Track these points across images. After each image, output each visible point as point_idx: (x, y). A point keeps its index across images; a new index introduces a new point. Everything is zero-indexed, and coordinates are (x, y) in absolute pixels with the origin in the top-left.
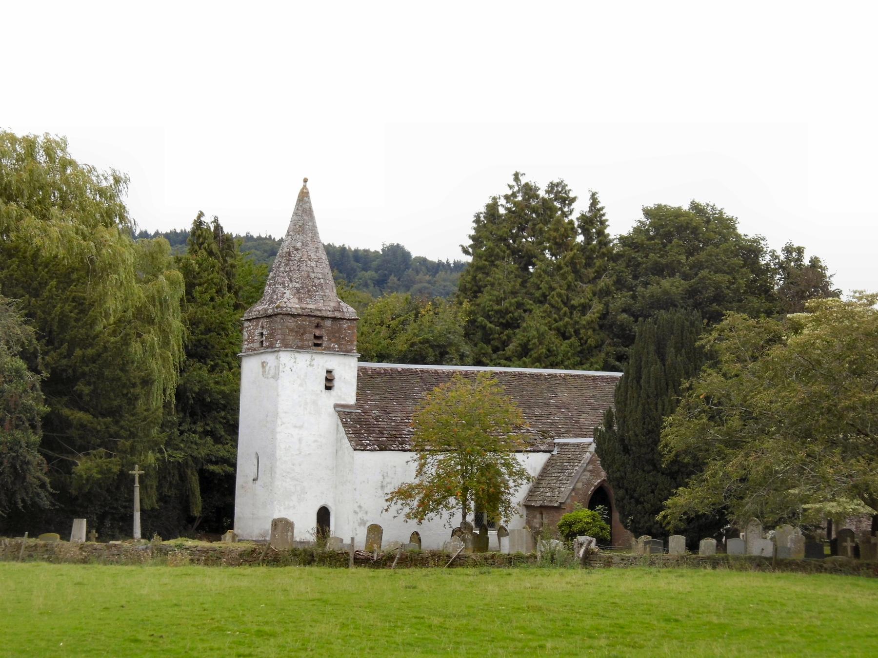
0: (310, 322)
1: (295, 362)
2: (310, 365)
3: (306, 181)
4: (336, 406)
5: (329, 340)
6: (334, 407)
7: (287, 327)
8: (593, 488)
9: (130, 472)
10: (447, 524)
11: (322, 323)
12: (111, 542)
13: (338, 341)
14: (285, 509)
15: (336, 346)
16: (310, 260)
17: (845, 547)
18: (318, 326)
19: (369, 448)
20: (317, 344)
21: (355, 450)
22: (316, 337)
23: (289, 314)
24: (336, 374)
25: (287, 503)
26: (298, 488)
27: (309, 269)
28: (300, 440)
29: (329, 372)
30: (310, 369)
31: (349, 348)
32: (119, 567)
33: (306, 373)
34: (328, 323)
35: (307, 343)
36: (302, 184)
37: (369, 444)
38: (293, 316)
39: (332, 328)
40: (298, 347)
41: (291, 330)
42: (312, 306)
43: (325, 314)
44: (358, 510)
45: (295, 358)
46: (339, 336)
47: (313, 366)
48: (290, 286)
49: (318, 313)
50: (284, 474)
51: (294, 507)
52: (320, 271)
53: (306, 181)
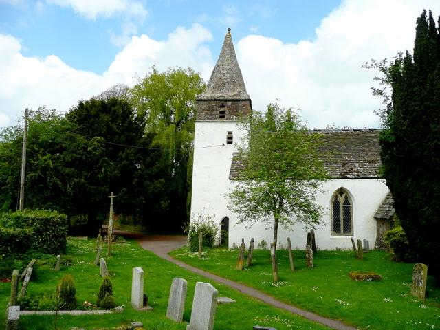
0: (216, 104)
3: (229, 30)
9: (54, 215)
17: (110, 198)
20: (222, 116)
21: (230, 179)
22: (221, 113)
24: (234, 135)
27: (221, 75)
29: (230, 133)
32: (159, 255)
34: (229, 104)
36: (241, 242)
40: (208, 119)
42: (219, 95)
43: (226, 98)
49: (223, 98)
53: (229, 30)
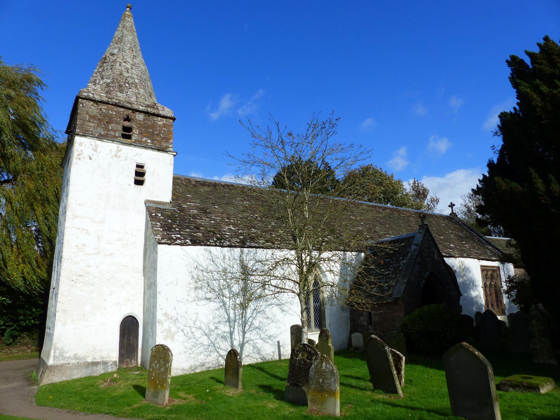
2: (116, 156)
4: (147, 202)
7: (87, 113)
8: (424, 281)
11: (132, 115)
13: (151, 136)
15: (149, 141)
16: (125, 62)
18: (127, 119)
19: (178, 241)
23: (90, 100)
29: (139, 166)
31: (164, 145)
37: (179, 239)
38: (95, 101)
39: (145, 123)
41: (91, 117)
46: (153, 133)
47: (119, 157)
48: (101, 82)
49: (129, 106)
50: (74, 278)
52: (135, 72)
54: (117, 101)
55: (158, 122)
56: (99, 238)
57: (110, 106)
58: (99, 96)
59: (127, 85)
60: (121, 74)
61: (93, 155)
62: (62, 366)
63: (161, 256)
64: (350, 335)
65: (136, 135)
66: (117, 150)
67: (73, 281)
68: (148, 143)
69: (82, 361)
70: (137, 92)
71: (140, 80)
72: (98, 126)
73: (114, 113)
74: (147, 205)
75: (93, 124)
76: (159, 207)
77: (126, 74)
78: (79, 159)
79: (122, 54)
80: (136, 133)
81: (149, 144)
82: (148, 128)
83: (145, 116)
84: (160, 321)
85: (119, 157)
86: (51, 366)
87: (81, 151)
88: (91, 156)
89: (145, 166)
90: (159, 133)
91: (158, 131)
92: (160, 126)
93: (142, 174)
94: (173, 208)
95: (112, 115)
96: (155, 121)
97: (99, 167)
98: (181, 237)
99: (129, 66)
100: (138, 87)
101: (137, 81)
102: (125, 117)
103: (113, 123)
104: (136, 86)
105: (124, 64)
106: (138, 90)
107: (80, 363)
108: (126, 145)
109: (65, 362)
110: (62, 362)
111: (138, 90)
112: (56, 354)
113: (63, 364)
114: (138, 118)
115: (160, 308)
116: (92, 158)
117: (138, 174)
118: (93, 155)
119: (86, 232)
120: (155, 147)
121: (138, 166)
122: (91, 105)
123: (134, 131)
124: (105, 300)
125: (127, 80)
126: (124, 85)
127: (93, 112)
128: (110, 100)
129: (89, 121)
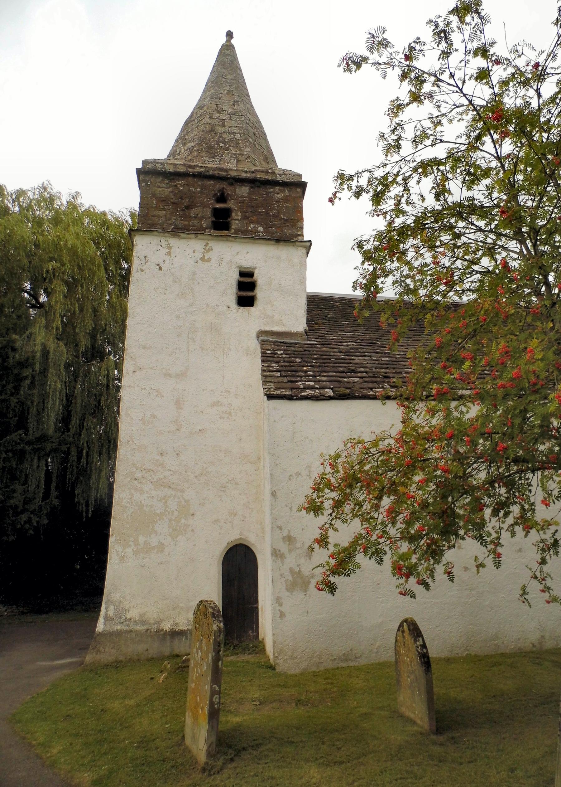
0: (203, 187)
1: (169, 254)
2: (203, 259)
4: (261, 333)
5: (245, 217)
6: (258, 337)
10: (534, 587)
11: (229, 190)
12: (38, 663)
14: (136, 553)
15: (261, 229)
16: (219, 112)
24: (260, 278)
25: (141, 539)
26: (173, 505)
28: (179, 404)
30: (203, 266)
33: (194, 274)
35: (196, 222)
36: (223, 40)
39: (251, 199)
44: (283, 548)
45: (169, 247)
46: (267, 213)
47: (209, 260)
50: (138, 475)
51: (161, 548)
53: (230, 35)
54: (203, 170)
55: (276, 195)
56: (179, 404)
57: (190, 179)
58: (172, 166)
59: (221, 145)
60: (212, 130)
61: (164, 261)
62: (119, 633)
63: (275, 421)
64: (217, 659)
65: (237, 222)
66: (205, 249)
67: (136, 479)
68: (260, 232)
69: (154, 628)
70: (238, 152)
71: (244, 134)
72: (172, 213)
73: (198, 189)
74: (261, 338)
75: (164, 212)
76: (282, 341)
77: (220, 130)
78: (142, 271)
79: (215, 102)
80: (236, 217)
81: (261, 234)
82: (258, 207)
83: (252, 187)
84: (278, 552)
85: (209, 260)
86: (100, 634)
87: (145, 257)
88: (162, 265)
89: (256, 272)
90: (279, 213)
91: (277, 210)
92: (278, 202)
93: (252, 286)
94: (308, 342)
95: (194, 193)
96: (270, 193)
97: (176, 282)
98: (315, 384)
99: (224, 116)
100: (241, 145)
101: (238, 136)
102: (216, 194)
103: (197, 206)
104: (237, 144)
105: (217, 115)
106: (241, 150)
107: (151, 632)
108: (220, 238)
109: (124, 628)
110: (119, 627)
111: (241, 150)
112: (109, 613)
113: (120, 631)
114: (240, 193)
115: (278, 527)
116: (164, 267)
117: (241, 286)
118: (164, 261)
119: (157, 394)
120: (273, 237)
121: (242, 274)
122: (159, 182)
123: (233, 214)
124: (193, 515)
125: (221, 137)
126: (216, 146)
127: (162, 193)
128: (190, 170)
129: (157, 208)
